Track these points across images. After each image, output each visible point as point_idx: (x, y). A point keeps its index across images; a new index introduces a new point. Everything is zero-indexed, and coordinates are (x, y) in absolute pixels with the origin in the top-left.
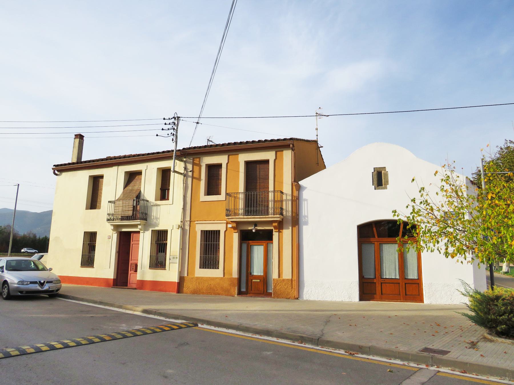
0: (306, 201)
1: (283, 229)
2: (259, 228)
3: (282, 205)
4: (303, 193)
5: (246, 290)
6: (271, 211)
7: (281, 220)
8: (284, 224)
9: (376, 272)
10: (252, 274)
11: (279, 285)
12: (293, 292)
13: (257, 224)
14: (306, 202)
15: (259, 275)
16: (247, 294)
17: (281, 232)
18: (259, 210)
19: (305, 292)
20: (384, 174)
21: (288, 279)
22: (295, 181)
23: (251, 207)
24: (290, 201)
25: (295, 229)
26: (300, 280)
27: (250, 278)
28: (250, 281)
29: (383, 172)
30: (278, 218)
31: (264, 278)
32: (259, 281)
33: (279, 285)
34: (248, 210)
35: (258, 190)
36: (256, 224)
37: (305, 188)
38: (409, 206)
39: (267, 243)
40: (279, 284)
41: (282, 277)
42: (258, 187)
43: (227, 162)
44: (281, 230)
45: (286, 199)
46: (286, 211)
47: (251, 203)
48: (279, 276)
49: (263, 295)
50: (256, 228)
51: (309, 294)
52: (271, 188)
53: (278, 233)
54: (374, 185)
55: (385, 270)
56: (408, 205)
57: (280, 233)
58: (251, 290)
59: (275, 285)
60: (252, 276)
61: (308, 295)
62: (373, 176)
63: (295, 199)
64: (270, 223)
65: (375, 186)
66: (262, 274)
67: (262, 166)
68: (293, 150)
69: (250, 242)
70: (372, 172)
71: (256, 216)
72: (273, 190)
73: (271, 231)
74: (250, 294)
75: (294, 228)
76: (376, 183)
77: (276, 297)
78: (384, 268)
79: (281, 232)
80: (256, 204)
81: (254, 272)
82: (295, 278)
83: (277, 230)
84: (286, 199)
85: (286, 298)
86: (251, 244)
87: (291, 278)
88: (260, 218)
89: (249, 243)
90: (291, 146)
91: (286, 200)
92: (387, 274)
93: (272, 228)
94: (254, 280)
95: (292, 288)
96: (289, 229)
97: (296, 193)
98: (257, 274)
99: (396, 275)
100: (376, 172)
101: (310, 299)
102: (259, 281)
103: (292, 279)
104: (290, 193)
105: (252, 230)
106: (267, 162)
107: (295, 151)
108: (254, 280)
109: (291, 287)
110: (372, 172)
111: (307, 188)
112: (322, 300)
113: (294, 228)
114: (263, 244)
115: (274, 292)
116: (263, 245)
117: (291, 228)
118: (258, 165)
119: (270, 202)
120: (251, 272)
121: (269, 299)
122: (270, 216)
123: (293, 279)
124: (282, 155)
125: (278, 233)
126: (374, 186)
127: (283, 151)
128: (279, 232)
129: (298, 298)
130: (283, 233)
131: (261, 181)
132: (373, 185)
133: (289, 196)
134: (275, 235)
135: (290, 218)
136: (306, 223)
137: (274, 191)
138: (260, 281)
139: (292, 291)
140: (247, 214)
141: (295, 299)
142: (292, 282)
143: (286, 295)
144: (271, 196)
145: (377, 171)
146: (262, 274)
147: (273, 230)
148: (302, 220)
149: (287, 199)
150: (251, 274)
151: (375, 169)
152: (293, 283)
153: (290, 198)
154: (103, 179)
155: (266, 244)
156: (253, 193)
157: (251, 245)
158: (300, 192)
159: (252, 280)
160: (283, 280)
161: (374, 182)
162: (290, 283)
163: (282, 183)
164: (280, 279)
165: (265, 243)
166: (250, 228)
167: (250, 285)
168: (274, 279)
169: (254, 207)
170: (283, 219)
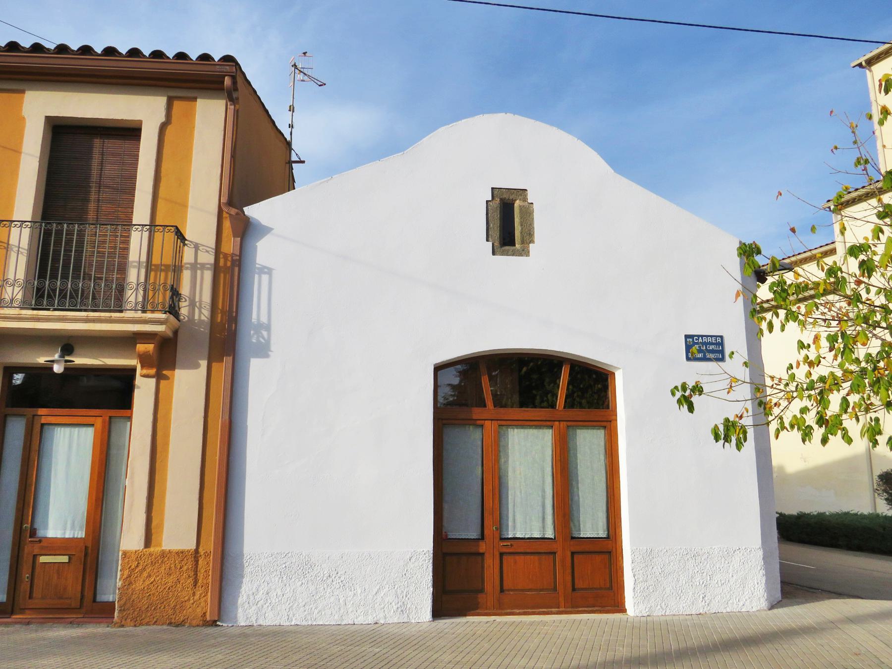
0: (265, 273)
1: (173, 367)
2: (80, 360)
6: (132, 296)
7: (170, 334)
10: (41, 533)
11: (145, 574)
12: (197, 597)
14: (265, 278)
15: (67, 536)
16: (12, 613)
17: (166, 378)
19: (245, 598)
21: (182, 552)
22: (230, 203)
24: (208, 269)
25: (222, 369)
32: (65, 559)
33: (145, 574)
39: (110, 417)
40: (144, 569)
41: (160, 545)
44: (164, 372)
45: (193, 261)
53: (153, 381)
54: (490, 239)
57: (163, 383)
58: (30, 597)
59: (129, 576)
60: (40, 541)
64: (127, 341)
67: (112, 145)
69: (42, 411)
70: (487, 202)
73: (126, 378)
74: (22, 611)
76: (496, 233)
79: (166, 378)
82: (209, 545)
83: (153, 371)
84: (193, 261)
85: (170, 624)
86: (44, 420)
87: (193, 547)
93: (132, 362)
94: (43, 559)
95: (195, 586)
96: (197, 366)
97: (230, 245)
101: (261, 622)
102: (65, 559)
103: (197, 551)
104: (210, 240)
108: (43, 559)
109: (190, 581)
110: (487, 202)
111: (273, 232)
114: (90, 420)
115: (122, 602)
116: (93, 425)
117: (204, 363)
120: (36, 526)
123: (201, 550)
124: (190, 116)
125: (153, 381)
126: (490, 244)
128: (159, 377)
132: (487, 240)
133: (207, 251)
138: (70, 559)
139: (194, 594)
141: (203, 625)
142: (197, 562)
145: (501, 200)
147: (133, 370)
148: (248, 337)
150: (33, 532)
152: (200, 567)
153: (207, 258)
155: (104, 422)
156: (65, 226)
157: (42, 425)
159: (35, 557)
160: (164, 554)
161: (490, 233)
162: (190, 565)
164: (152, 549)
165: (99, 417)
168: (125, 553)
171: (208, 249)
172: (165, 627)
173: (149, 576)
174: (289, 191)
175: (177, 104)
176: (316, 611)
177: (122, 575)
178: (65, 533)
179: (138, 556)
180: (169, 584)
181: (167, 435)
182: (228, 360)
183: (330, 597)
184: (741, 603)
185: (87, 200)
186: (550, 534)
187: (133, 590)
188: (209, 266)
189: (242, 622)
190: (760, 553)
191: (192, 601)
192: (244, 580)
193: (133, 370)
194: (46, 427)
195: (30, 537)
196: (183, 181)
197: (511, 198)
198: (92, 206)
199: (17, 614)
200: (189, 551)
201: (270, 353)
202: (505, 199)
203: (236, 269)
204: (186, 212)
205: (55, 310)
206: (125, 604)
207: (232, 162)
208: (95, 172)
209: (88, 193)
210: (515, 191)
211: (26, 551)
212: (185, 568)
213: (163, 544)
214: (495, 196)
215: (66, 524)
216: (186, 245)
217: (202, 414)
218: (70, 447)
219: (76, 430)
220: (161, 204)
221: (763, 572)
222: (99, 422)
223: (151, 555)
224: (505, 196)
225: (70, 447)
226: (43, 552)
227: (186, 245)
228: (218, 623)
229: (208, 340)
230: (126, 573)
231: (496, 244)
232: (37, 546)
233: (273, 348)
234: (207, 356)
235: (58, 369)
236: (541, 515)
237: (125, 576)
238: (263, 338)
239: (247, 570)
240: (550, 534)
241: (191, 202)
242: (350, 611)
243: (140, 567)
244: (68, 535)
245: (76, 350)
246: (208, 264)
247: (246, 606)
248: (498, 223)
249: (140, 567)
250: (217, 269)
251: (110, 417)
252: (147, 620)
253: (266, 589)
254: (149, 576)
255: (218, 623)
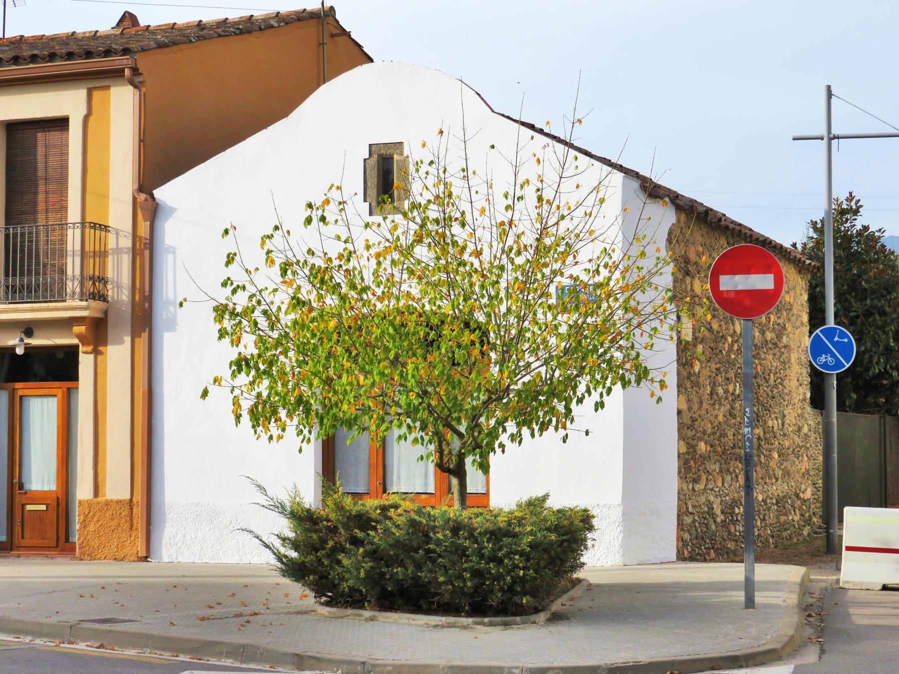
0: (171, 252)
1: (105, 344)
2: (35, 342)
3: (103, 266)
4: (164, 227)
5: (7, 538)
6: (72, 286)
7: (99, 315)
8: (109, 328)
9: (21, 532)
10: (27, 487)
11: (95, 519)
12: (133, 538)
13: (31, 326)
14: (170, 257)
15: (45, 489)
16: (11, 550)
17: (101, 353)
18: (29, 286)
19: (167, 539)
20: (398, 164)
21: (120, 501)
22: (141, 189)
23: (22, 274)
24: (125, 253)
25: (142, 342)
26: (156, 500)
27: (17, 499)
28: (17, 508)
29: (396, 157)
30: (85, 309)
31: (58, 498)
32: (43, 507)
33: (95, 519)
34: (13, 287)
35: (41, 217)
36: (28, 329)
37: (173, 210)
38: (184, 304)
39: (68, 389)
40: (94, 515)
41: (105, 496)
42: (41, 206)
43: (84, 112)
44: (100, 348)
45: (115, 247)
46: (119, 286)
47: (22, 259)
48: (96, 493)
49: (57, 551)
50: (27, 341)
51: (178, 545)
52: (74, 214)
53: (92, 356)
54: (368, 199)
55: (399, 467)
56: (185, 300)
57: (99, 357)
58: (23, 538)
59: (84, 521)
60: (26, 493)
61: (174, 547)
62: (368, 171)
63: (140, 246)
64: (67, 324)
65: (370, 205)
66: (53, 487)
67: (54, 136)
68: (132, 83)
69: (18, 385)
70: (365, 160)
71: (51, 302)
72: (79, 221)
73: (71, 353)
74: (19, 547)
75: (137, 340)
76: (373, 192)
77: (86, 556)
78: (395, 462)
79: (101, 353)
80: (37, 264)
81: (31, 483)
82: (138, 497)
83: (90, 348)
84: (115, 247)
85: (115, 559)
86: (20, 393)
87: (129, 497)
88: (33, 310)
89: (14, 389)
90: (127, 72)
91: (118, 251)
92: (403, 482)
93: (75, 341)
94: (29, 507)
95: (131, 529)
96: (122, 342)
97: (143, 229)
98: (40, 489)
99: (426, 484)
100: (376, 156)
101: (180, 559)
102: (43, 507)
103: (131, 500)
104: (128, 226)
105: (13, 348)
106: (61, 123)
107: (143, 90)
108: (29, 507)
109: (128, 525)
110: (365, 160)
111: (175, 215)
112: (213, 562)
113: (137, 340)
114: (54, 391)
115: (80, 541)
116: (55, 396)
117: (128, 340)
118: (39, 135)
119: (70, 255)
120: (23, 481)
121: (67, 560)
122: (69, 303)
123: (134, 499)
124: (106, 104)
125: (92, 356)
126: (367, 204)
127: (108, 87)
128: (96, 352)
129: (146, 557)
130: (106, 357)
131: (51, 187)
132: (365, 201)
133: (125, 236)
134: (86, 362)
135: (127, 309)
136: (172, 325)
137: (83, 224)
138: (47, 507)
139: (131, 535)
140: (12, 299)
141: (138, 561)
142: (132, 509)
143: (115, 550)
144: (73, 239)
145: (379, 156)
146: (53, 487)
147: (77, 346)
148: (161, 315)
149: (120, 246)
150: (21, 486)
151: (374, 149)
152: (134, 513)
153: (126, 242)
154: (67, 130)
155: (63, 392)
156: (11, 230)
157: (21, 397)
158: (158, 223)
159: (23, 505)
160: (108, 503)
161: (368, 192)
162: (125, 512)
163: (108, 198)
164: (99, 499)
165: (59, 387)
166: (11, 342)
167: (18, 520)
168: (80, 502)
169: (22, 274)
170: (106, 312)
171: (126, 234)
172: (111, 561)
173: (98, 521)
174: (324, 83)
175: (96, 94)
176: (221, 552)
177: (79, 519)
178: (43, 487)
179: (90, 504)
180: (113, 527)
181: (105, 404)
182: (145, 335)
183: (231, 541)
184: (596, 559)
185: (36, 193)
186: (431, 489)
187: (88, 532)
188: (125, 250)
189: (166, 559)
190: (620, 510)
191: (129, 542)
192: (166, 525)
193: (76, 347)
194: (24, 398)
195: (19, 490)
196: (104, 173)
197: (388, 153)
198: (41, 197)
199: (16, 551)
200: (125, 501)
201: (177, 327)
202: (383, 154)
203: (147, 252)
204: (107, 206)
205: (10, 303)
206: (83, 542)
207: (142, 149)
208: (40, 166)
209: (36, 186)
210: (392, 145)
211: (17, 501)
212: (123, 514)
213: (107, 494)
214: (373, 152)
215: (43, 479)
216: (109, 231)
217: (129, 384)
218: (42, 415)
219: (45, 400)
220: (88, 196)
221: (621, 528)
222: (60, 392)
223: (98, 503)
224: (383, 152)
225: (42, 415)
226: (28, 502)
227: (109, 231)
228: (149, 559)
229: (130, 318)
230: (82, 517)
231: (373, 204)
232: (24, 497)
233: (179, 323)
234: (130, 334)
235: (20, 351)
236: (423, 471)
237: (81, 521)
238: (171, 314)
239: (169, 516)
240: (431, 489)
241: (111, 196)
242: (247, 553)
243: (91, 514)
244: (46, 488)
245: (36, 333)
246: (124, 248)
247: (169, 546)
248: (375, 181)
249: (91, 514)
250: (134, 251)
251: (68, 389)
252: (99, 556)
253: (183, 532)
254: (98, 521)
255: (149, 559)
